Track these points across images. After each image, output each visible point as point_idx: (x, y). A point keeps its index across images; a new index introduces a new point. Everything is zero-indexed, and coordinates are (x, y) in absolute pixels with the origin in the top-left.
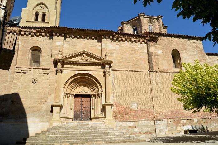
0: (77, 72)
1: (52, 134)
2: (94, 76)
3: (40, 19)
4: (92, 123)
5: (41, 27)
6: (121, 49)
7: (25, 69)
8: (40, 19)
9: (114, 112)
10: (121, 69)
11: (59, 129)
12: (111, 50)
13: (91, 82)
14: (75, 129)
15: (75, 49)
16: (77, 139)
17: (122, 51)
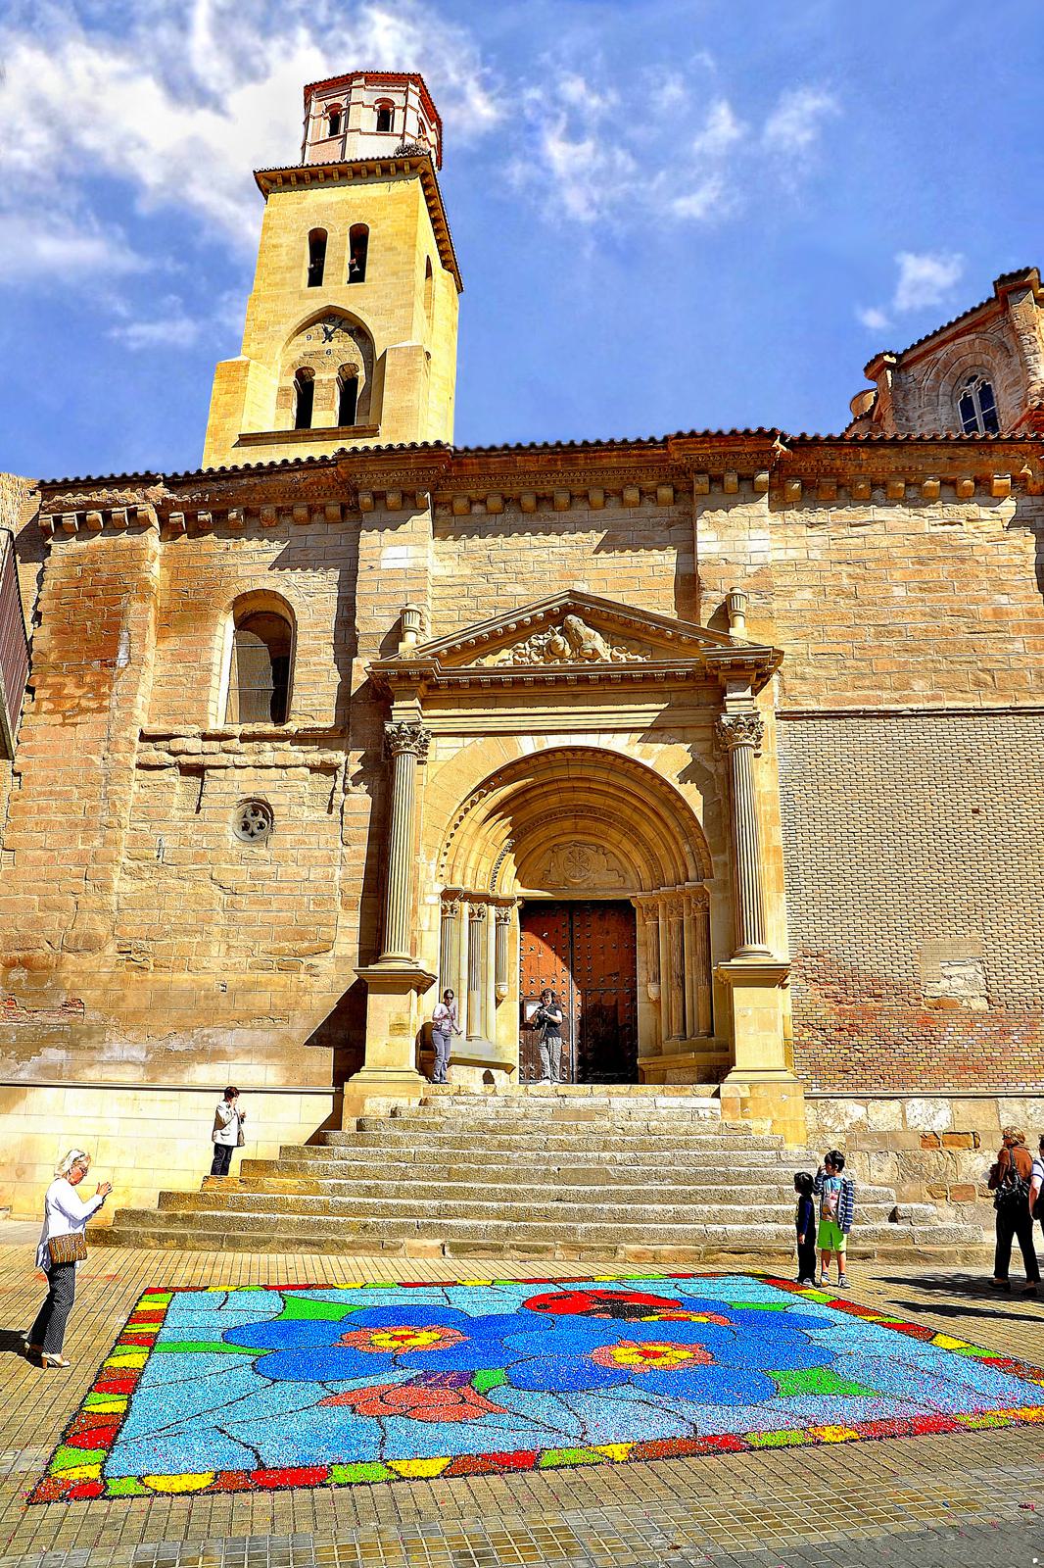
0: (528, 746)
1: (346, 1173)
2: (647, 770)
3: (325, 416)
4: (630, 1103)
5: (223, 469)
6: (843, 557)
7: (195, 745)
8: (325, 416)
9: (804, 1021)
10: (852, 701)
11: (396, 1142)
12: (763, 570)
13: (635, 809)
14: (501, 1146)
15: (510, 588)
16: (500, 1215)
17: (850, 569)
